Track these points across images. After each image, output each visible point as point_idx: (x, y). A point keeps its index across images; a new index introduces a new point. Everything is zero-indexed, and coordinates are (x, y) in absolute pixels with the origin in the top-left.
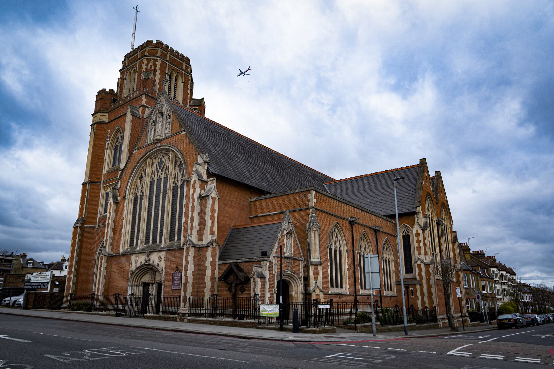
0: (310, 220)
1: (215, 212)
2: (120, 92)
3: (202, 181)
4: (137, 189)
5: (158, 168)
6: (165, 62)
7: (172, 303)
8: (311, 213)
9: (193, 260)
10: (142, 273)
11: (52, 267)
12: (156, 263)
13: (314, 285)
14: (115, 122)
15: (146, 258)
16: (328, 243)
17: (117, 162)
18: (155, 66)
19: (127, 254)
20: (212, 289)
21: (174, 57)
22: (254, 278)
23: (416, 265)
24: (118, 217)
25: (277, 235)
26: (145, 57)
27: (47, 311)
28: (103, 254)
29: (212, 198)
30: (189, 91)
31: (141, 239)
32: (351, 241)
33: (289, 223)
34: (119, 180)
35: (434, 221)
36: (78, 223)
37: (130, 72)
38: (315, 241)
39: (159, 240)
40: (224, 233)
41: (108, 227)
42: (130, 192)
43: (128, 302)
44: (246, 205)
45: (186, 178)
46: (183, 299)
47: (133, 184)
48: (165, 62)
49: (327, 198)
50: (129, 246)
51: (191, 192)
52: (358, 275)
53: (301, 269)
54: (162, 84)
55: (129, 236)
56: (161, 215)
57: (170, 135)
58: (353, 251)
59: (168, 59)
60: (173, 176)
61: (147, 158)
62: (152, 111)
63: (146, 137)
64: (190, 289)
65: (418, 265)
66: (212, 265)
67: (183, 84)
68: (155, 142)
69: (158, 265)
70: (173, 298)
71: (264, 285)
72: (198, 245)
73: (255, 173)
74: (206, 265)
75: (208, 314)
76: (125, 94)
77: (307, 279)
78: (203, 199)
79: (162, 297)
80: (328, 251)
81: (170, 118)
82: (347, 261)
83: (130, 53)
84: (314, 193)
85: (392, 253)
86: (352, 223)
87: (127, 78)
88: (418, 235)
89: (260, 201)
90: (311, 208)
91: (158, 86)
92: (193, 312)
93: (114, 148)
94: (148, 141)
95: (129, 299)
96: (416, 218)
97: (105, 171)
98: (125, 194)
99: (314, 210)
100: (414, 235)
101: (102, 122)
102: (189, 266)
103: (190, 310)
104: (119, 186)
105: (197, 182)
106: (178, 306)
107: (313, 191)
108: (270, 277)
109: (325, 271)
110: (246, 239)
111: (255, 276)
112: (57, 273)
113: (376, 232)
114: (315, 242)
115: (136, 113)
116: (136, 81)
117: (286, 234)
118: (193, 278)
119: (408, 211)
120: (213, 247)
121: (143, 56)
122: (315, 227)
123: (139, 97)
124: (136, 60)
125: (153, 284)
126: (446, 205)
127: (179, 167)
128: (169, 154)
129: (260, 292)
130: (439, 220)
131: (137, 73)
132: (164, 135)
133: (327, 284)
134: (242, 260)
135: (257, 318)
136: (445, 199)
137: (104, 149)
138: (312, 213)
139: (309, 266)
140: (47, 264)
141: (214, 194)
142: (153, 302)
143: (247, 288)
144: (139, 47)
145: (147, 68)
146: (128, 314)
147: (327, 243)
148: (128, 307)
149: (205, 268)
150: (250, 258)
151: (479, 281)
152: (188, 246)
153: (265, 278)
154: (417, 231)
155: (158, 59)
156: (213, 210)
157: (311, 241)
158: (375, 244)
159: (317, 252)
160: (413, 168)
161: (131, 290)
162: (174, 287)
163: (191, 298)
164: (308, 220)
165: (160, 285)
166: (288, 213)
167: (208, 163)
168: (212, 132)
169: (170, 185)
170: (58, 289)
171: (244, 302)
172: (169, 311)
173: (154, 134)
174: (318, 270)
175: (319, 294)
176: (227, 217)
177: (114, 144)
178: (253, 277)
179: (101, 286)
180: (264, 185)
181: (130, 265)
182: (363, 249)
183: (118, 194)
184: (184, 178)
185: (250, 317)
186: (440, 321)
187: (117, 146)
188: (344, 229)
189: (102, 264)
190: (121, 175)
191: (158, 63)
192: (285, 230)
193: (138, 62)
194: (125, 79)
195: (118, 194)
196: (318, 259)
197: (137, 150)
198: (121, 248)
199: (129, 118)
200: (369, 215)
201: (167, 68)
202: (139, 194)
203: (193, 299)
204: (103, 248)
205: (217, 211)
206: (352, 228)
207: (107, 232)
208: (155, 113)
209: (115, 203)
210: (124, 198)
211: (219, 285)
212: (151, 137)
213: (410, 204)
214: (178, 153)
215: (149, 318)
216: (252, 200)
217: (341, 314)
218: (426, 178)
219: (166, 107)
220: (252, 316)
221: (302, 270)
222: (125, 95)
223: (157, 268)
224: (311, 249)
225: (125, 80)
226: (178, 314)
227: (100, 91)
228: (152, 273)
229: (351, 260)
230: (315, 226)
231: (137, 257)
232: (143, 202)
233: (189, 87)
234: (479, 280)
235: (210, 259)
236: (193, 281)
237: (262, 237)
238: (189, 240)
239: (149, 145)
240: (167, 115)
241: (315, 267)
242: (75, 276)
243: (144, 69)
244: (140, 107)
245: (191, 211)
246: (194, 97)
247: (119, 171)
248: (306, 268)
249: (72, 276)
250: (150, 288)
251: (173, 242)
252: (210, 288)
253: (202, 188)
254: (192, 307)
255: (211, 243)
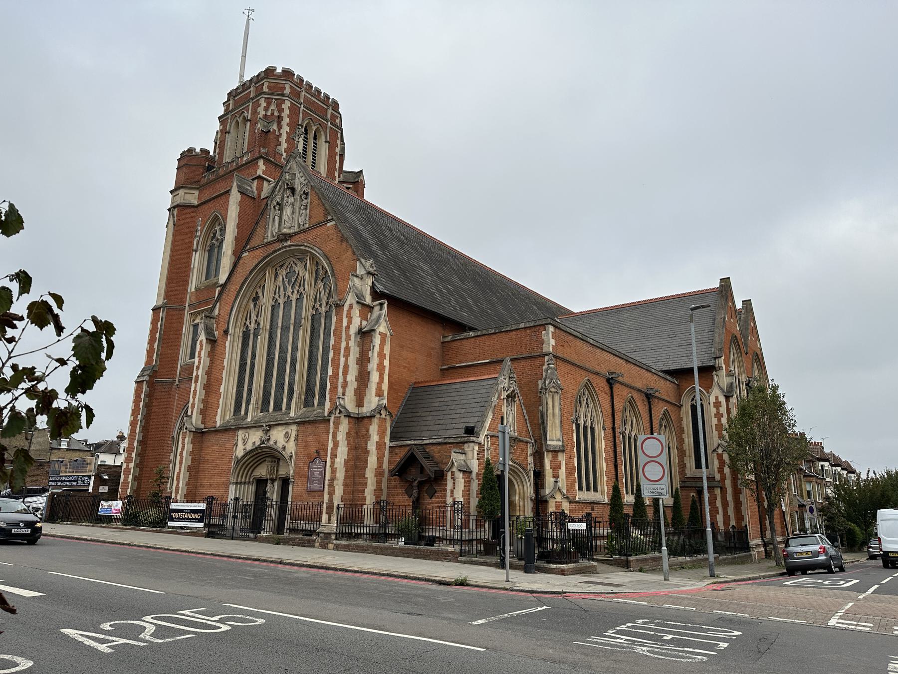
0: (544, 374)
1: (385, 359)
2: (219, 154)
3: (363, 305)
4: (248, 317)
5: (287, 283)
6: (297, 104)
7: (308, 515)
8: (546, 363)
9: (347, 439)
10: (254, 462)
11: (101, 450)
12: (280, 445)
13: (552, 485)
14: (211, 204)
15: (263, 436)
16: (574, 414)
17: (213, 273)
18: (281, 110)
19: (229, 430)
20: (378, 491)
21: (313, 98)
22: (452, 472)
23: (715, 454)
24: (214, 365)
25: (490, 398)
26: (263, 96)
27: (87, 526)
28: (186, 429)
29: (380, 333)
30: (338, 158)
31: (255, 403)
32: (609, 411)
33: (510, 378)
34: (217, 302)
35: (743, 383)
36: (145, 375)
37: (237, 121)
38: (553, 410)
39: (287, 405)
40: (399, 394)
41: (196, 381)
42: (236, 322)
43: (228, 512)
44: (436, 348)
45: (336, 300)
46: (327, 508)
47: (242, 310)
48: (297, 104)
49: (572, 338)
50: (232, 414)
51: (345, 323)
52: (622, 470)
53: (529, 457)
54: (293, 139)
55: (234, 397)
56: (291, 363)
57: (307, 226)
58: (614, 429)
59: (302, 100)
60: (312, 297)
61: (267, 266)
62: (275, 187)
63: (266, 230)
64: (339, 491)
65: (717, 454)
66: (379, 449)
67: (328, 144)
68: (281, 238)
69: (284, 448)
70: (309, 506)
71: (469, 484)
72: (354, 413)
73: (450, 295)
74: (369, 447)
75: (371, 534)
76: (227, 158)
77: (539, 476)
78: (365, 335)
79: (289, 503)
80: (574, 428)
81: (306, 198)
82: (604, 446)
83: (237, 88)
84: (551, 329)
85: (674, 433)
86: (611, 381)
87: (231, 131)
88: (717, 405)
89: (459, 341)
90: (547, 355)
91: (284, 145)
92: (344, 532)
93: (208, 248)
94: (269, 235)
95: (231, 506)
96: (715, 377)
97: (192, 288)
98: (228, 327)
99: (552, 358)
100: (712, 405)
101: (188, 203)
102: (339, 449)
103: (338, 527)
104: (216, 312)
105: (355, 306)
106: (318, 520)
107: (550, 326)
108: (479, 471)
109: (570, 462)
110: (437, 404)
111: (454, 469)
112: (108, 459)
113: (649, 397)
114: (553, 413)
115: (247, 189)
116: (248, 136)
117: (505, 397)
118: (345, 471)
119: (701, 365)
120: (382, 417)
121: (260, 93)
122: (553, 387)
123: (253, 162)
124: (248, 99)
125: (273, 481)
126: (760, 356)
127: (253, 301)
128: (305, 260)
129: (463, 496)
130: (749, 380)
131: (249, 123)
132: (296, 226)
133: (572, 484)
134: (431, 441)
135: (457, 544)
136: (759, 346)
137: (189, 251)
138: (547, 363)
139: (544, 454)
140: (92, 444)
141: (382, 328)
142: (272, 512)
143: (440, 489)
144: (252, 79)
145: (266, 114)
146: (230, 533)
147: (572, 415)
148: (229, 520)
149: (367, 453)
150: (445, 438)
151: (803, 482)
152: (338, 415)
153: (471, 472)
154: (717, 398)
155: (284, 100)
156: (381, 356)
157: (547, 410)
158: (648, 418)
159: (556, 429)
160: (708, 294)
161: (234, 492)
162: (310, 488)
163: (342, 506)
164: (542, 375)
165: (285, 482)
166: (509, 363)
167: (373, 275)
168: (377, 225)
169: (307, 311)
170: (107, 488)
171: (316, 511)
172: (301, 528)
173: (280, 225)
174: (559, 459)
175: (561, 502)
176: (405, 367)
177: (209, 243)
178: (451, 470)
179: (182, 485)
180: (464, 316)
181: (234, 448)
182: (628, 427)
183: (215, 325)
184: (331, 300)
185: (445, 542)
186: (753, 550)
187: (214, 244)
188: (600, 392)
189: (185, 446)
190: (220, 294)
191: (286, 105)
192: (504, 391)
193: (251, 104)
194: (229, 133)
195: (215, 325)
196: (559, 440)
197: (249, 250)
198: (218, 418)
199: (235, 197)
200: (638, 368)
201: (301, 116)
202: (252, 327)
203: (344, 508)
204: (187, 418)
205: (388, 358)
206: (611, 388)
207: (195, 391)
208: (280, 188)
209: (209, 341)
210: (226, 332)
211: (389, 483)
212: (272, 230)
213: (704, 353)
214: (321, 258)
215: (267, 540)
216: (446, 340)
217: (600, 537)
218: (730, 309)
219: (301, 179)
220: (450, 540)
221: (530, 460)
222: (227, 159)
223: (281, 454)
224: (547, 424)
225: (227, 134)
226: (318, 534)
227: (184, 152)
228: (272, 462)
229: (611, 444)
230: (554, 385)
231: (247, 435)
232: (259, 341)
233: (338, 150)
234: (802, 480)
235: (375, 438)
236: (345, 476)
237: (465, 402)
238: (340, 404)
239: (270, 243)
240: (302, 192)
241: (554, 455)
242: (136, 466)
243: (261, 116)
244: (253, 180)
245: (344, 356)
246: (346, 168)
247: (218, 287)
248: (539, 456)
249: (132, 465)
250: (268, 487)
251: (310, 409)
252: (375, 488)
253: (363, 317)
254: (342, 521)
255: (378, 410)
